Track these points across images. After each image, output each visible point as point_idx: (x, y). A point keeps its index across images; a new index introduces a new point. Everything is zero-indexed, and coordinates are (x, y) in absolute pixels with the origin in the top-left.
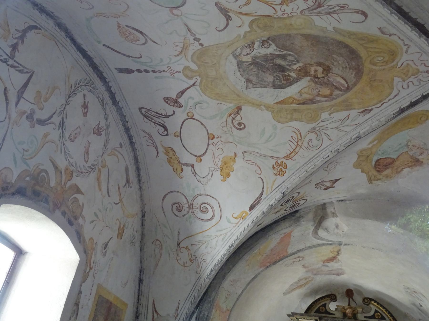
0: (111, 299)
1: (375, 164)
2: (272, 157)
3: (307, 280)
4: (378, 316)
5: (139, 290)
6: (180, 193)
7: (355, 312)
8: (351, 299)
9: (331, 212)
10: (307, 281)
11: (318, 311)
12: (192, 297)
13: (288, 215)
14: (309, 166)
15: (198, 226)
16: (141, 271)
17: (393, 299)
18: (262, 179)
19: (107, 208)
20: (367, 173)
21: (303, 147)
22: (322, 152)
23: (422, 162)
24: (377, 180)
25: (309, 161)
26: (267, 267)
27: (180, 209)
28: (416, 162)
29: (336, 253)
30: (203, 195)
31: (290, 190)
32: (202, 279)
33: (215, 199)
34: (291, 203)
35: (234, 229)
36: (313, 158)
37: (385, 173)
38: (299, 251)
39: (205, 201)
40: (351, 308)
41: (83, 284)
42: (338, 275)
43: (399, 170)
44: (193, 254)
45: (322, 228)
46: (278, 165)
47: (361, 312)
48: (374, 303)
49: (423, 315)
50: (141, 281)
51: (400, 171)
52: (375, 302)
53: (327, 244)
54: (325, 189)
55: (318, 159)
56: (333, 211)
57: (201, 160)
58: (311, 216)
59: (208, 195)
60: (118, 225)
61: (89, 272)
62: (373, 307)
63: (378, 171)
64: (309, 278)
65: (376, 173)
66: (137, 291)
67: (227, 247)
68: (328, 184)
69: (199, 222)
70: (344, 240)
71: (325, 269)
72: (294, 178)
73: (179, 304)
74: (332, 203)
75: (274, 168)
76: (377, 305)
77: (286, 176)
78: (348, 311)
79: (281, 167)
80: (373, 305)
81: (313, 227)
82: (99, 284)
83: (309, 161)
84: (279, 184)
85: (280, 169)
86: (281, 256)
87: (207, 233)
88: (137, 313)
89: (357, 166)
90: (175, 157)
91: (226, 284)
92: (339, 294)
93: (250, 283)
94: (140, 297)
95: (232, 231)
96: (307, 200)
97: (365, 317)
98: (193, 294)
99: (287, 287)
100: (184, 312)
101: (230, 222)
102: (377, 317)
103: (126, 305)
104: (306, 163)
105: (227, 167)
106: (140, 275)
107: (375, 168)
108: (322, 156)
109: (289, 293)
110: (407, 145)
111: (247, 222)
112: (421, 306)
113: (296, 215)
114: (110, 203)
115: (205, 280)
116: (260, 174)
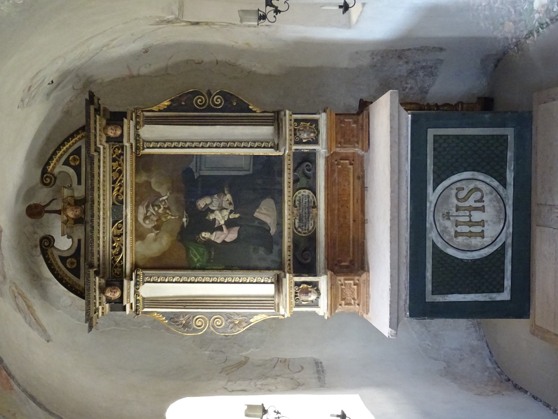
3: (17, 294)
4: (75, 159)
7: (72, 202)
8: (47, 209)
11: (76, 272)
26: (9, 374)
40: (65, 209)
47: (70, 191)
48: (51, 167)
49: (65, 82)
52: (48, 164)
64: (13, 291)
76: (54, 161)
78: (71, 214)
92: (35, 233)
93: (46, 410)
97: (79, 183)
99: (34, 335)
102: (77, 163)
109: (45, 331)
112: (52, 82)
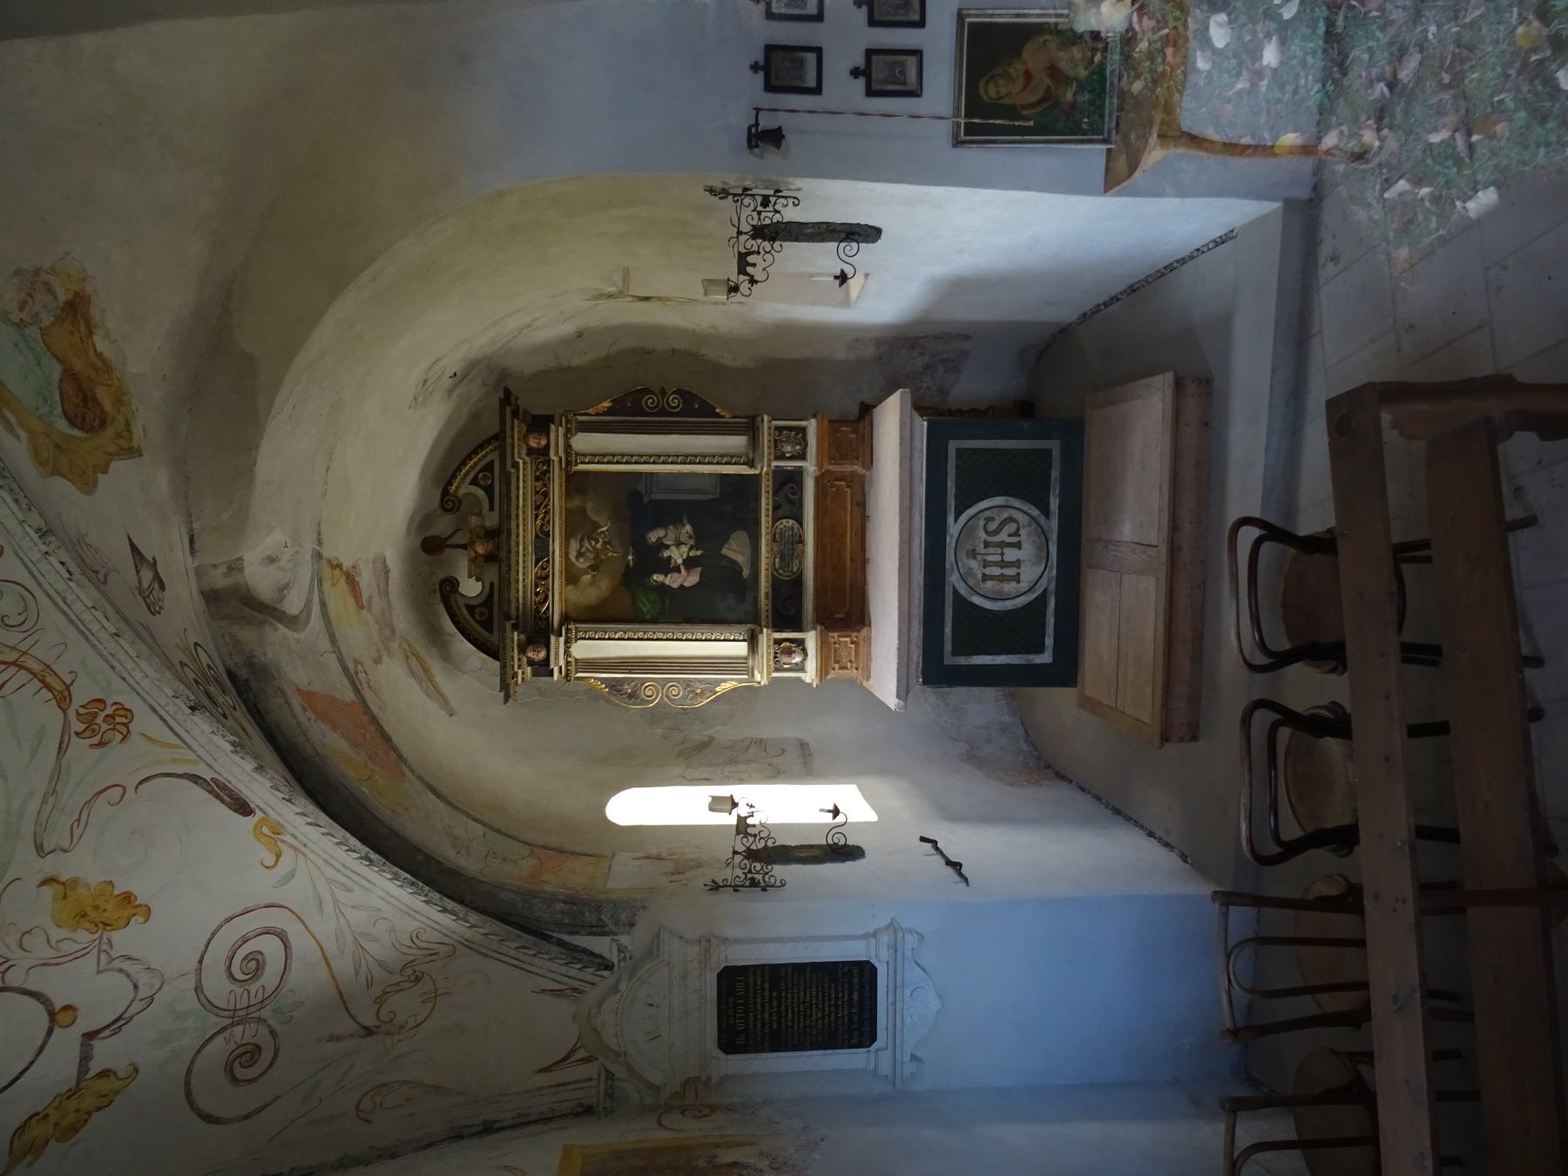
1: (81, 429)
2: (61, 750)
4: (485, 477)
5: (514, 1127)
6: (192, 1063)
9: (225, 575)
10: (410, 655)
11: (488, 625)
13: (245, 702)
14: (95, 627)
15: (308, 978)
16: (457, 1136)
17: (438, 439)
18: (141, 783)
20: (111, 457)
21: (23, 647)
22: (46, 586)
23: (77, 294)
24: (130, 432)
25: (77, 628)
26: (400, 757)
27: (250, 1053)
28: (76, 309)
30: (199, 981)
31: (182, 687)
32: (469, 934)
33: (213, 934)
34: (212, 689)
35: (311, 855)
36: (66, 615)
37: (108, 406)
38: (345, 669)
39: (223, 968)
43: (99, 364)
46: (90, 728)
50: (488, 1129)
51: (104, 361)
52: (450, 483)
53: (321, 592)
54: (162, 587)
55: (70, 598)
56: (223, 569)
57: (68, 1008)
58: (246, 634)
59: (200, 962)
62: (463, 489)
63: (103, 423)
65: (109, 433)
67: (371, 873)
68: (147, 576)
69: (294, 978)
71: (377, 603)
72: (138, 676)
73: (543, 991)
74: (199, 573)
75: (101, 744)
77: (130, 701)
78: (480, 549)
79: (99, 720)
81: (279, 626)
83: (77, 628)
84: (160, 723)
85: (105, 723)
86: (365, 718)
87: (331, 948)
88: (577, 1115)
89: (87, 484)
90: (51, 1111)
91: (470, 864)
93: (449, 803)
94: (532, 1118)
95: (321, 863)
96: (196, 644)
97: (492, 508)
98: (512, 953)
99: (433, 707)
100: (563, 970)
101: (291, 875)
103: (568, 1151)
104: (87, 639)
105: (96, 908)
106: (473, 1135)
107: (92, 430)
108: (61, 586)
109: (446, 701)
110: (20, 325)
113: (245, 676)
115: (473, 926)
116: (124, 788)
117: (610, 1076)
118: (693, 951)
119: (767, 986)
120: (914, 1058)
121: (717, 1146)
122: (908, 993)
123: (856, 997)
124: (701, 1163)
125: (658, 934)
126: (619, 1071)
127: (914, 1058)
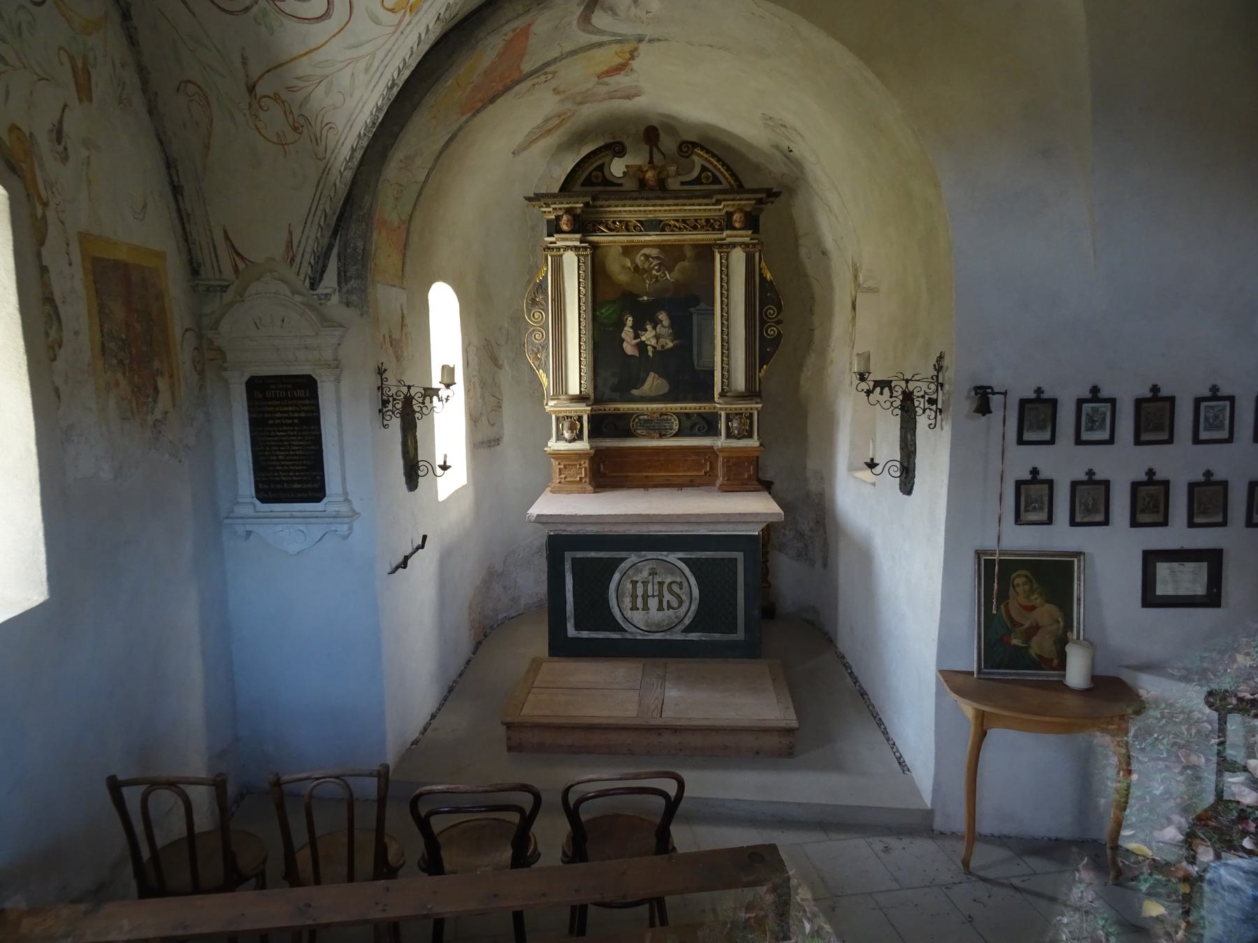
0: (122, 255)
4: (708, 178)
5: (179, 210)
7: (662, 176)
8: (655, 149)
10: (562, 118)
11: (588, 182)
12: (319, 213)
19: (19, 27)
26: (478, 111)
29: (628, 56)
32: (335, 172)
35: (394, 38)
38: (548, 64)
41: (43, 249)
42: (629, 97)
44: (296, 112)
45: (603, 9)
50: (176, 190)
52: (703, 148)
53: (610, 42)
60: (68, 66)
61: (44, 217)
62: (698, 159)
66: (175, 215)
67: (381, 88)
70: (648, 32)
71: (603, 90)
73: (291, 233)
78: (649, 175)
80: (699, 155)
81: (582, 8)
82: (79, 233)
87: (318, 57)
88: (191, 262)
91: (392, 171)
94: (187, 226)
95: (388, 45)
97: (683, 183)
98: (321, 207)
99: (519, 138)
100: (309, 249)
101: (377, 22)
103: (161, 255)
106: (171, 177)
111: (424, 21)
114: (21, 7)
115: (341, 174)
117: (224, 289)
118: (328, 354)
119: (303, 415)
120: (249, 533)
121: (171, 376)
122: (301, 527)
123: (296, 486)
124: (156, 364)
125: (342, 326)
126: (229, 296)
127: (249, 533)
